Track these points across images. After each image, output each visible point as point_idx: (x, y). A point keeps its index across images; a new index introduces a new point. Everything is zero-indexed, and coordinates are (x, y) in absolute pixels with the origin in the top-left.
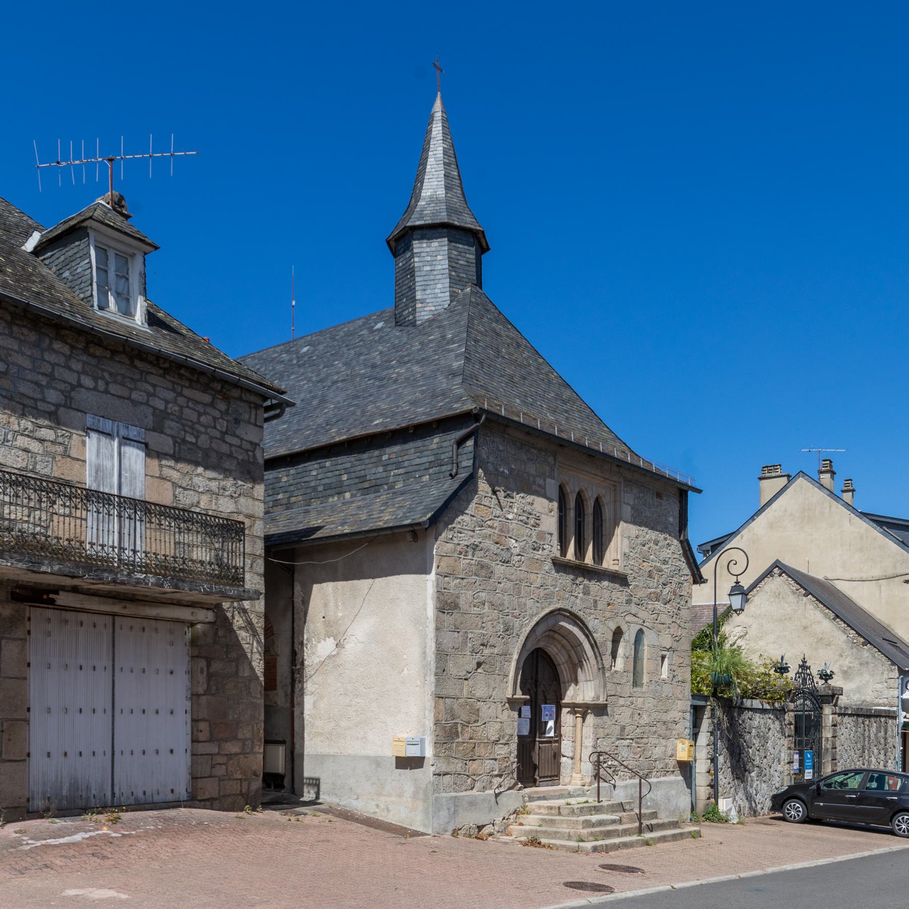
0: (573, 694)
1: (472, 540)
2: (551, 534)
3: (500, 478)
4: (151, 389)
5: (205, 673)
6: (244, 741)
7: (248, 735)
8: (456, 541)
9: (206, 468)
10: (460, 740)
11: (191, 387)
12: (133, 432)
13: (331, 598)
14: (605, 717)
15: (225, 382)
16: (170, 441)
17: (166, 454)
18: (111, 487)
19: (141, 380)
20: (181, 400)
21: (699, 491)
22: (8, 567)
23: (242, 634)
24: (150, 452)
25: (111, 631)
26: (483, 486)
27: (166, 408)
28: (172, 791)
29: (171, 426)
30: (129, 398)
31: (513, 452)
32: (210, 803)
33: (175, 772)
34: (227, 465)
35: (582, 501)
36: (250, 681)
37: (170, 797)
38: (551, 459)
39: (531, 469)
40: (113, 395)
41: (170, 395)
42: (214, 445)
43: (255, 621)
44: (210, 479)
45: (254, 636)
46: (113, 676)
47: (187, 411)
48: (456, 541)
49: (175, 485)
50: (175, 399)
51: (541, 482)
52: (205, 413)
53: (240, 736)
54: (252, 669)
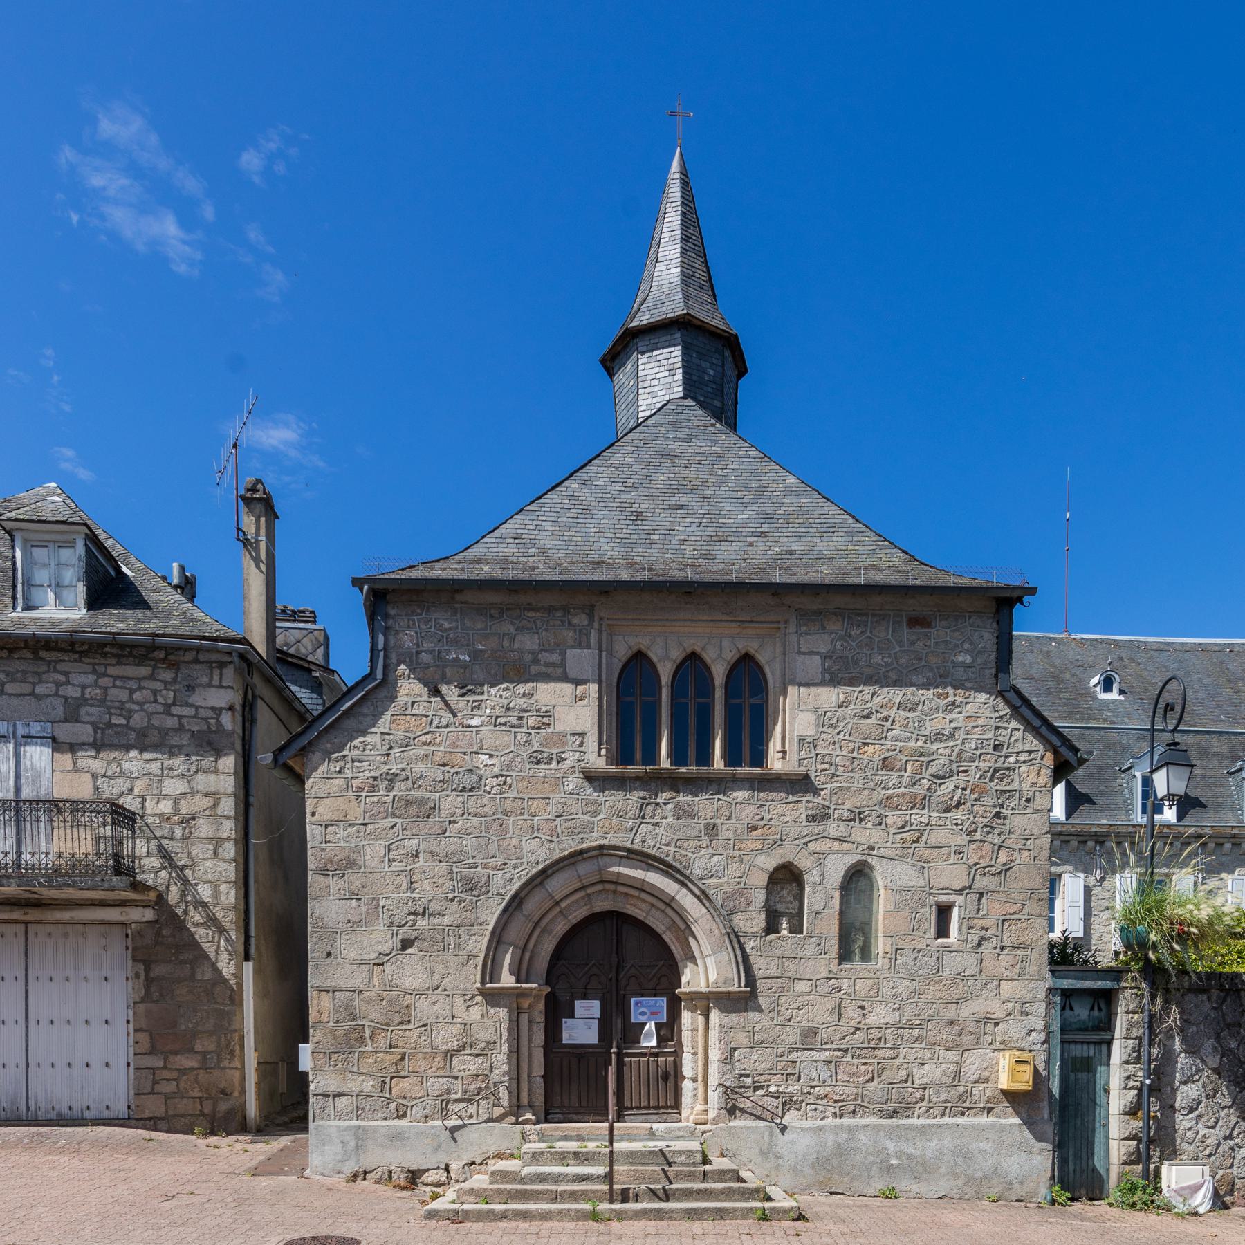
0: (693, 979)
1: (384, 769)
4: (62, 678)
5: (142, 977)
6: (204, 1054)
7: (212, 1047)
8: (349, 774)
9: (142, 751)
10: (369, 1048)
11: (119, 663)
12: (36, 729)
14: (752, 1015)
15: (170, 650)
16: (90, 729)
17: (84, 744)
18: (7, 791)
19: (48, 671)
20: (104, 681)
22: (10, 890)
23: (201, 933)
24: (57, 745)
25: (23, 939)
26: (409, 689)
27: (83, 694)
28: (107, 1107)
29: (91, 712)
30: (33, 694)
32: (152, 1123)
33: (113, 1084)
34: (175, 740)
36: (214, 984)
37: (106, 1114)
38: (580, 620)
39: (528, 642)
40: (10, 695)
41: (90, 679)
42: (155, 722)
43: (219, 915)
44: (148, 761)
45: (221, 933)
46: (26, 985)
47: (113, 693)
48: (349, 774)
49: (95, 776)
50: (96, 681)
52: (140, 688)
53: (198, 1047)
54: (218, 972)
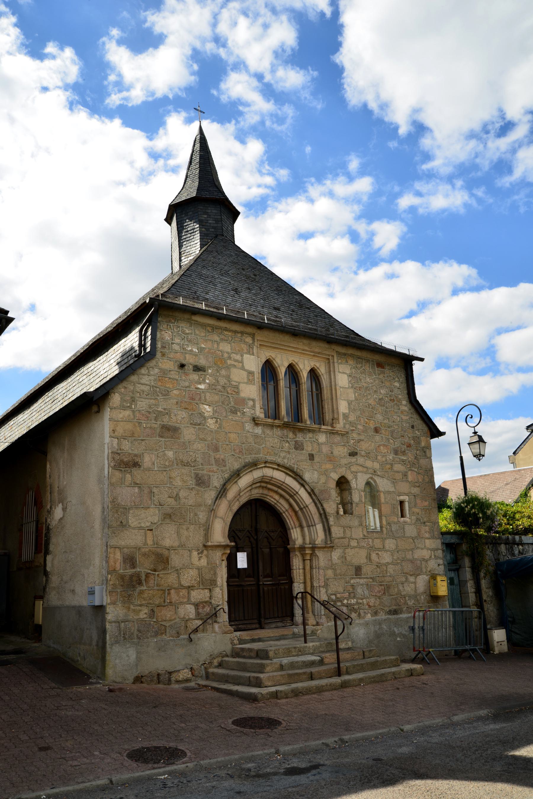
2: (253, 400)
3: (187, 355)
13: (62, 473)
21: (422, 360)
31: (203, 334)
35: (296, 373)
38: (249, 340)
39: (226, 347)
51: (238, 357)
